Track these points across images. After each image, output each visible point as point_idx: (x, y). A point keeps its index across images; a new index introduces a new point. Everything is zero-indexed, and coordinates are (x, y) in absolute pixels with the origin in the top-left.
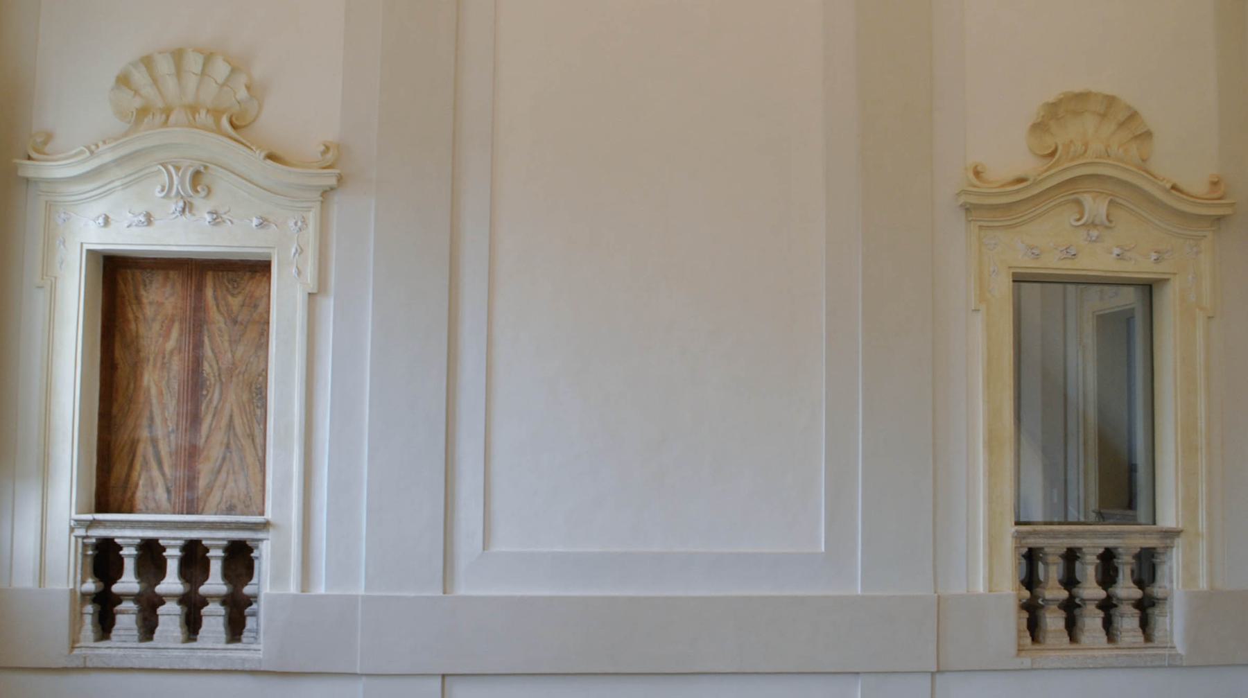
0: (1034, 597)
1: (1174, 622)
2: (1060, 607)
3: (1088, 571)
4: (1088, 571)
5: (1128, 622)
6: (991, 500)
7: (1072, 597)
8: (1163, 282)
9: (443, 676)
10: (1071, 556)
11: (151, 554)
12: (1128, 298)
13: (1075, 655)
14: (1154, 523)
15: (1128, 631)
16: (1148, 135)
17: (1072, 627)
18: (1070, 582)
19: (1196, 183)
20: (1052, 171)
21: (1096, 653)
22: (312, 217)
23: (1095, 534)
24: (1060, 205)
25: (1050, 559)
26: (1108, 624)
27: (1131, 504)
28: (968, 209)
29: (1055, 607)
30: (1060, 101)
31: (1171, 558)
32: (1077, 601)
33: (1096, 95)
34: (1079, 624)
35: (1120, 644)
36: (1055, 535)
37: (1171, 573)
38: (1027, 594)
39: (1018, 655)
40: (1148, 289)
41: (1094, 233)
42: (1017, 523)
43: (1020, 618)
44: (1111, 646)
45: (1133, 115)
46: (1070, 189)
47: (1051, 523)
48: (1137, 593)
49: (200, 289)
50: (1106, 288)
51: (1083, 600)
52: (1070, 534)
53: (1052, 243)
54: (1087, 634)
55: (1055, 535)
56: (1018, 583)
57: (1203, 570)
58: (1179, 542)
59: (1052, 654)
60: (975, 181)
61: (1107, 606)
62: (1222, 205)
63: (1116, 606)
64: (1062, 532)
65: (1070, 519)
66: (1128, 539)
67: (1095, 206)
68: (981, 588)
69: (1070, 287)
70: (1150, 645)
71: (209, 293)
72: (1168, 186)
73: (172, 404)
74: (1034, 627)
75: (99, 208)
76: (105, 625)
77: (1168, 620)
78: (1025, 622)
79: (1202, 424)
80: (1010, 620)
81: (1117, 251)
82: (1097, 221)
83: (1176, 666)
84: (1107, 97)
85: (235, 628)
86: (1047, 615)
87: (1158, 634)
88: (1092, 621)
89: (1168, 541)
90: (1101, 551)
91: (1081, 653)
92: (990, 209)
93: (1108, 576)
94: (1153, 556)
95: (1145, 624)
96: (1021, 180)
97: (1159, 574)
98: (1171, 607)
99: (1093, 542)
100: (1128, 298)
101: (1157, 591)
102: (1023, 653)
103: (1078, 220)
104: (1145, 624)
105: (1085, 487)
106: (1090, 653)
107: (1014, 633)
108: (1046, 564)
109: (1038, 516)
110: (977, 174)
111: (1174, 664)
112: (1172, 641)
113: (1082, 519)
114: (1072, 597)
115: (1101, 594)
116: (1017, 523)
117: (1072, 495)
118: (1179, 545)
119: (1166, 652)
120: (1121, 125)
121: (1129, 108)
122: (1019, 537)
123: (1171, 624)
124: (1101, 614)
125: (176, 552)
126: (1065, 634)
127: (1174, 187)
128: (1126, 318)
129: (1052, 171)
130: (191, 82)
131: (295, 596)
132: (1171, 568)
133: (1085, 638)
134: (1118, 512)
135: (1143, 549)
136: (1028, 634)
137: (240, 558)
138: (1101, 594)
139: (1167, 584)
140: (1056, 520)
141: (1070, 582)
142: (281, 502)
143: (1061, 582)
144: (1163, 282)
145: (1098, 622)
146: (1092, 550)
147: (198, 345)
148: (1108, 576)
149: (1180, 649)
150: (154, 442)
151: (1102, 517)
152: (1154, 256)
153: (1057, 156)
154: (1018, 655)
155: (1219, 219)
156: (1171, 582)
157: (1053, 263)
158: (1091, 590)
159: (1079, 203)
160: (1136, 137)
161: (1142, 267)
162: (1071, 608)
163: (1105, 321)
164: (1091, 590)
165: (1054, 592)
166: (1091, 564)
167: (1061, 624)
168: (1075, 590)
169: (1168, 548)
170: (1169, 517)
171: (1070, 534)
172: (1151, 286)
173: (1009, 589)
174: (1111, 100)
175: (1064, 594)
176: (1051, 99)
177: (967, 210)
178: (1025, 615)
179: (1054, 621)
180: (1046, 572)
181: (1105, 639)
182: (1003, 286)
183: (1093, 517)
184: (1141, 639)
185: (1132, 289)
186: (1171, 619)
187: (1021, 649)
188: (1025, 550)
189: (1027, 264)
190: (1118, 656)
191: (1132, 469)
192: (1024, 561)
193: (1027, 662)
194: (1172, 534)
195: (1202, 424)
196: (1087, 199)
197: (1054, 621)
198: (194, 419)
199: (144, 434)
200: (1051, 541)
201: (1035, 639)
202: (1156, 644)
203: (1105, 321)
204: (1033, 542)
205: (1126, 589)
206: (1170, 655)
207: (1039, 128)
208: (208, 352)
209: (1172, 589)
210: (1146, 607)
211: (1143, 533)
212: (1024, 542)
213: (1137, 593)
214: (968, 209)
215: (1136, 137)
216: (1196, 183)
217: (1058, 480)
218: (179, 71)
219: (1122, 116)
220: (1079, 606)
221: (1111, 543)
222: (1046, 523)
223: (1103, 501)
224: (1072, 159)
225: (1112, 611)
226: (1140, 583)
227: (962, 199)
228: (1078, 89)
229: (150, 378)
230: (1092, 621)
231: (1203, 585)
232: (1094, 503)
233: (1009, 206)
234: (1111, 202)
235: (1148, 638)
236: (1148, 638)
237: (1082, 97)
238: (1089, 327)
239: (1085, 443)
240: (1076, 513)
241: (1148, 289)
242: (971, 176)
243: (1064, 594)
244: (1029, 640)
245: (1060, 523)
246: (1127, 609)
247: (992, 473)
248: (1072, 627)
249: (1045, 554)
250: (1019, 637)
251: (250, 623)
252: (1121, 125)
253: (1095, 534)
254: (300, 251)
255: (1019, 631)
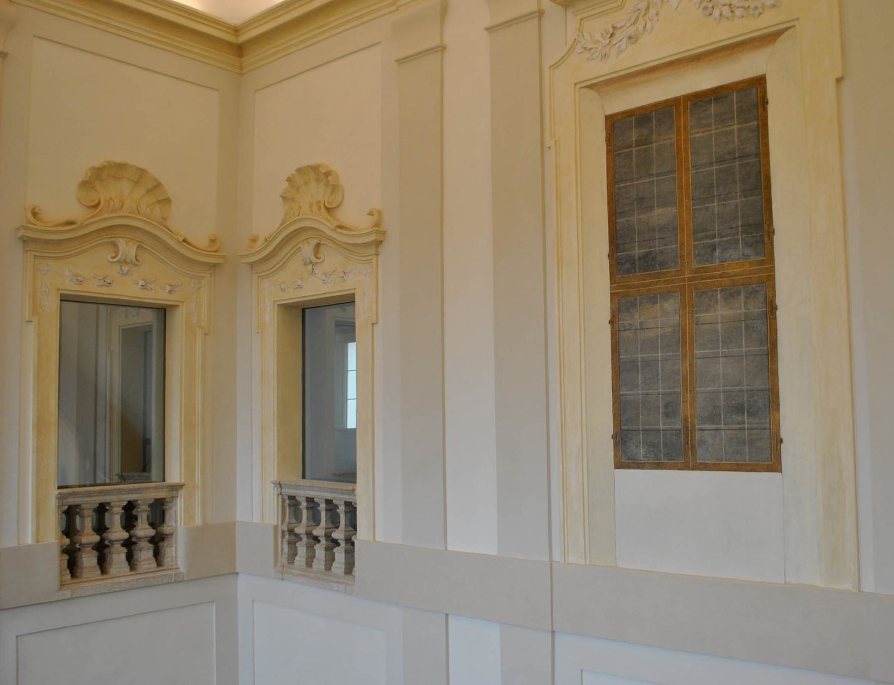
0: (73, 543)
1: (178, 551)
2: (93, 548)
3: (115, 520)
4: (115, 520)
5: (145, 554)
6: (38, 471)
7: (102, 540)
8: (174, 307)
10: (102, 510)
11: (102, 510)
12: (148, 318)
13: (106, 583)
14: (164, 481)
15: (144, 560)
16: (168, 201)
17: (102, 563)
18: (101, 528)
19: (200, 239)
20: (96, 219)
21: (122, 579)
23: (120, 492)
24: (96, 246)
25: (86, 513)
26: (130, 557)
27: (145, 467)
28: (25, 241)
29: (89, 549)
30: (104, 167)
31: (176, 504)
32: (106, 542)
33: (131, 166)
34: (108, 559)
35: (139, 571)
36: (89, 494)
37: (176, 517)
38: (67, 541)
39: (60, 589)
40: (163, 312)
41: (126, 268)
42: (59, 488)
43: (61, 560)
44: (133, 573)
45: (158, 185)
46: (109, 234)
47: (85, 486)
48: (151, 532)
50: (131, 309)
51: (112, 542)
52: (102, 493)
53: (92, 272)
54: (114, 566)
55: (89, 494)
56: (60, 534)
57: (198, 511)
58: (182, 493)
59: (87, 584)
60: (33, 220)
61: (129, 544)
62: (213, 256)
63: (135, 543)
64: (95, 492)
65: (98, 482)
66: (144, 493)
67: (127, 249)
68: (29, 540)
69: (101, 306)
70: (161, 568)
72: (181, 239)
74: (73, 566)
76: (73, 566)
77: (174, 548)
78: (66, 563)
79: (199, 408)
80: (55, 562)
81: (141, 283)
82: (128, 260)
83: (180, 581)
84: (138, 169)
86: (84, 556)
87: (167, 560)
88: (118, 556)
89: (174, 493)
90: (125, 503)
91: (110, 581)
92: (42, 242)
93: (129, 521)
94: (163, 505)
95: (157, 554)
96: (70, 223)
97: (167, 516)
98: (176, 539)
99: (118, 498)
100: (148, 318)
101: (166, 529)
102: (65, 587)
103: (114, 258)
104: (157, 554)
105: (110, 457)
106: (116, 580)
107: (57, 573)
108: (82, 517)
109: (72, 481)
110: (35, 214)
111: (179, 580)
112: (176, 564)
113: (108, 481)
114: (102, 540)
115: (125, 535)
116: (59, 488)
117: (100, 462)
119: (173, 572)
120: (149, 191)
121: (155, 179)
122: (61, 497)
123: (176, 551)
124: (125, 550)
125: (145, 507)
126: (98, 568)
127: (184, 241)
128: (145, 332)
129: (96, 219)
131: (30, 546)
132: (176, 512)
133: (113, 570)
134: (137, 474)
135: (156, 500)
136: (68, 572)
138: (125, 535)
139: (174, 524)
140: (88, 483)
141: (101, 528)
143: (94, 530)
144: (174, 307)
145: (123, 556)
146: (118, 503)
148: (129, 521)
149: (182, 569)
151: (123, 479)
152: (168, 288)
153: (100, 208)
154: (60, 589)
155: (215, 266)
156: (176, 522)
157: (93, 288)
158: (117, 533)
159: (115, 245)
160: (159, 202)
161: (159, 295)
162: (102, 550)
163: (128, 334)
164: (117, 533)
165: (89, 537)
166: (118, 513)
167: (94, 561)
168: (105, 535)
170: (174, 476)
171: (102, 493)
172: (165, 310)
173: (53, 538)
174: (142, 172)
175: (96, 538)
176: (97, 164)
177: (25, 242)
178: (66, 557)
179: (88, 560)
180: (83, 523)
181: (99, 572)
182: (52, 303)
183: (116, 479)
184: (155, 565)
185: (149, 312)
186: (176, 548)
187: (62, 584)
188: (66, 508)
189: (72, 288)
190: (138, 579)
191: (146, 442)
192: (64, 516)
193: (67, 593)
194: (176, 488)
195: (199, 408)
196: (121, 243)
197: (88, 560)
200: (87, 499)
201: (74, 575)
202: (165, 567)
203: (128, 334)
204: (72, 501)
205: (143, 530)
206: (176, 574)
207: (86, 185)
209: (176, 527)
210: (158, 542)
211: (156, 488)
212: (65, 501)
213: (151, 532)
214: (25, 241)
215: (159, 202)
216: (200, 239)
217: (89, 453)
220: (108, 546)
221: (132, 497)
222: (80, 486)
223: (124, 466)
224: (111, 212)
225: (133, 547)
226: (152, 525)
227: (21, 233)
228: (118, 160)
230: (118, 556)
231: (198, 521)
232: (117, 469)
233: (59, 242)
234: (139, 247)
235: (159, 564)
236: (159, 564)
237: (121, 166)
238: (116, 340)
239: (111, 424)
240: (103, 476)
241: (163, 312)
242: (30, 215)
243: (96, 538)
244: (69, 576)
245: (91, 485)
246: (117, 546)
247: (40, 449)
248: (102, 563)
249: (83, 509)
250: (61, 575)
252: (149, 191)
253: (120, 492)
255: (61, 571)
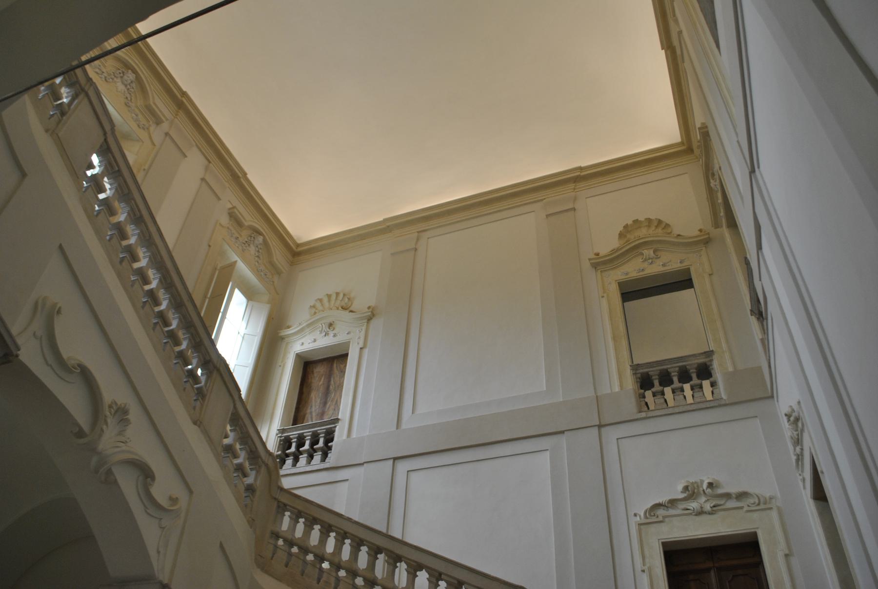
9: (395, 459)
22: (364, 328)
49: (332, 365)
68: (617, 389)
71: (335, 365)
73: (319, 401)
75: (301, 342)
85: (325, 456)
92: (601, 264)
118: (715, 358)
120: (657, 227)
130: (333, 302)
137: (330, 437)
142: (344, 413)
147: (329, 381)
149: (724, 397)
150: (311, 413)
169: (711, 361)
198: (325, 403)
199: (309, 411)
208: (332, 382)
218: (329, 301)
219: (663, 226)
229: (313, 395)
231: (731, 369)
251: (329, 455)
252: (657, 227)
254: (359, 338)
